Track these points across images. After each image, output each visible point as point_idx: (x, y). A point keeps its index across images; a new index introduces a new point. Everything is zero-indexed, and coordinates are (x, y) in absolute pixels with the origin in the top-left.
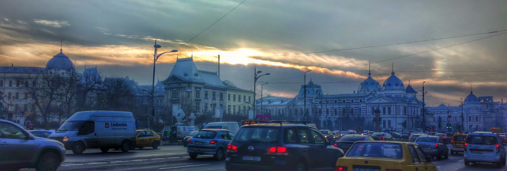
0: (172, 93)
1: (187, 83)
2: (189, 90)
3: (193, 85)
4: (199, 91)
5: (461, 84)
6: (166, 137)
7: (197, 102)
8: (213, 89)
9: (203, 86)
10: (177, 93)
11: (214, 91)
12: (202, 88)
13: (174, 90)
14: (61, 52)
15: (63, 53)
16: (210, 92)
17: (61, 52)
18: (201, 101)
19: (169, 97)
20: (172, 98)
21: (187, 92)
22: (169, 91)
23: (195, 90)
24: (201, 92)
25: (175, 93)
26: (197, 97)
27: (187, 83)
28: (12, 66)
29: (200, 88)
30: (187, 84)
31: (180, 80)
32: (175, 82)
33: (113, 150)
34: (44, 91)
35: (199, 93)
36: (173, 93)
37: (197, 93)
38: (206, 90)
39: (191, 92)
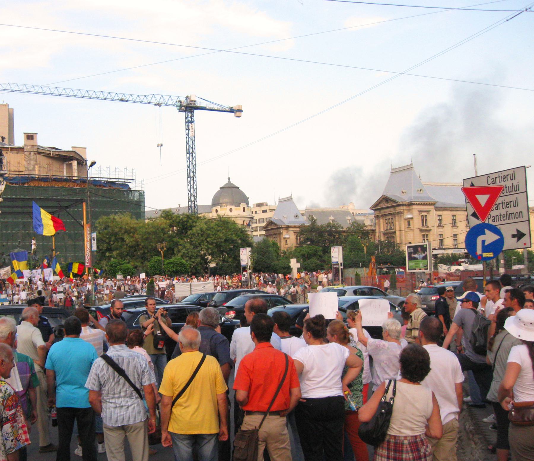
0: (385, 223)
1: (406, 205)
2: (409, 216)
3: (414, 207)
4: (426, 216)
5: (222, 418)
6: (170, 332)
7: (424, 234)
8: (450, 210)
9: (431, 207)
10: (392, 223)
11: (454, 213)
12: (432, 211)
13: (16, 251)
14: (229, 182)
15: (231, 182)
16: (447, 216)
17: (229, 182)
18: (431, 232)
19: (382, 230)
20: (387, 230)
21: (405, 219)
22: (381, 221)
23: (420, 214)
24: (429, 218)
25: (390, 223)
26: (423, 225)
27: (406, 205)
28: (179, 206)
29: (428, 211)
30: (405, 207)
31: (395, 201)
32: (388, 205)
33: (14, 373)
34: (388, 217)
35: (426, 220)
36: (387, 223)
37: (422, 220)
38: (440, 213)
39: (412, 219)
